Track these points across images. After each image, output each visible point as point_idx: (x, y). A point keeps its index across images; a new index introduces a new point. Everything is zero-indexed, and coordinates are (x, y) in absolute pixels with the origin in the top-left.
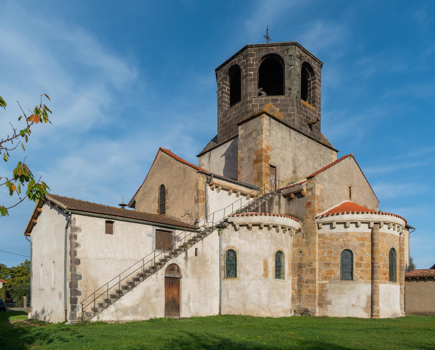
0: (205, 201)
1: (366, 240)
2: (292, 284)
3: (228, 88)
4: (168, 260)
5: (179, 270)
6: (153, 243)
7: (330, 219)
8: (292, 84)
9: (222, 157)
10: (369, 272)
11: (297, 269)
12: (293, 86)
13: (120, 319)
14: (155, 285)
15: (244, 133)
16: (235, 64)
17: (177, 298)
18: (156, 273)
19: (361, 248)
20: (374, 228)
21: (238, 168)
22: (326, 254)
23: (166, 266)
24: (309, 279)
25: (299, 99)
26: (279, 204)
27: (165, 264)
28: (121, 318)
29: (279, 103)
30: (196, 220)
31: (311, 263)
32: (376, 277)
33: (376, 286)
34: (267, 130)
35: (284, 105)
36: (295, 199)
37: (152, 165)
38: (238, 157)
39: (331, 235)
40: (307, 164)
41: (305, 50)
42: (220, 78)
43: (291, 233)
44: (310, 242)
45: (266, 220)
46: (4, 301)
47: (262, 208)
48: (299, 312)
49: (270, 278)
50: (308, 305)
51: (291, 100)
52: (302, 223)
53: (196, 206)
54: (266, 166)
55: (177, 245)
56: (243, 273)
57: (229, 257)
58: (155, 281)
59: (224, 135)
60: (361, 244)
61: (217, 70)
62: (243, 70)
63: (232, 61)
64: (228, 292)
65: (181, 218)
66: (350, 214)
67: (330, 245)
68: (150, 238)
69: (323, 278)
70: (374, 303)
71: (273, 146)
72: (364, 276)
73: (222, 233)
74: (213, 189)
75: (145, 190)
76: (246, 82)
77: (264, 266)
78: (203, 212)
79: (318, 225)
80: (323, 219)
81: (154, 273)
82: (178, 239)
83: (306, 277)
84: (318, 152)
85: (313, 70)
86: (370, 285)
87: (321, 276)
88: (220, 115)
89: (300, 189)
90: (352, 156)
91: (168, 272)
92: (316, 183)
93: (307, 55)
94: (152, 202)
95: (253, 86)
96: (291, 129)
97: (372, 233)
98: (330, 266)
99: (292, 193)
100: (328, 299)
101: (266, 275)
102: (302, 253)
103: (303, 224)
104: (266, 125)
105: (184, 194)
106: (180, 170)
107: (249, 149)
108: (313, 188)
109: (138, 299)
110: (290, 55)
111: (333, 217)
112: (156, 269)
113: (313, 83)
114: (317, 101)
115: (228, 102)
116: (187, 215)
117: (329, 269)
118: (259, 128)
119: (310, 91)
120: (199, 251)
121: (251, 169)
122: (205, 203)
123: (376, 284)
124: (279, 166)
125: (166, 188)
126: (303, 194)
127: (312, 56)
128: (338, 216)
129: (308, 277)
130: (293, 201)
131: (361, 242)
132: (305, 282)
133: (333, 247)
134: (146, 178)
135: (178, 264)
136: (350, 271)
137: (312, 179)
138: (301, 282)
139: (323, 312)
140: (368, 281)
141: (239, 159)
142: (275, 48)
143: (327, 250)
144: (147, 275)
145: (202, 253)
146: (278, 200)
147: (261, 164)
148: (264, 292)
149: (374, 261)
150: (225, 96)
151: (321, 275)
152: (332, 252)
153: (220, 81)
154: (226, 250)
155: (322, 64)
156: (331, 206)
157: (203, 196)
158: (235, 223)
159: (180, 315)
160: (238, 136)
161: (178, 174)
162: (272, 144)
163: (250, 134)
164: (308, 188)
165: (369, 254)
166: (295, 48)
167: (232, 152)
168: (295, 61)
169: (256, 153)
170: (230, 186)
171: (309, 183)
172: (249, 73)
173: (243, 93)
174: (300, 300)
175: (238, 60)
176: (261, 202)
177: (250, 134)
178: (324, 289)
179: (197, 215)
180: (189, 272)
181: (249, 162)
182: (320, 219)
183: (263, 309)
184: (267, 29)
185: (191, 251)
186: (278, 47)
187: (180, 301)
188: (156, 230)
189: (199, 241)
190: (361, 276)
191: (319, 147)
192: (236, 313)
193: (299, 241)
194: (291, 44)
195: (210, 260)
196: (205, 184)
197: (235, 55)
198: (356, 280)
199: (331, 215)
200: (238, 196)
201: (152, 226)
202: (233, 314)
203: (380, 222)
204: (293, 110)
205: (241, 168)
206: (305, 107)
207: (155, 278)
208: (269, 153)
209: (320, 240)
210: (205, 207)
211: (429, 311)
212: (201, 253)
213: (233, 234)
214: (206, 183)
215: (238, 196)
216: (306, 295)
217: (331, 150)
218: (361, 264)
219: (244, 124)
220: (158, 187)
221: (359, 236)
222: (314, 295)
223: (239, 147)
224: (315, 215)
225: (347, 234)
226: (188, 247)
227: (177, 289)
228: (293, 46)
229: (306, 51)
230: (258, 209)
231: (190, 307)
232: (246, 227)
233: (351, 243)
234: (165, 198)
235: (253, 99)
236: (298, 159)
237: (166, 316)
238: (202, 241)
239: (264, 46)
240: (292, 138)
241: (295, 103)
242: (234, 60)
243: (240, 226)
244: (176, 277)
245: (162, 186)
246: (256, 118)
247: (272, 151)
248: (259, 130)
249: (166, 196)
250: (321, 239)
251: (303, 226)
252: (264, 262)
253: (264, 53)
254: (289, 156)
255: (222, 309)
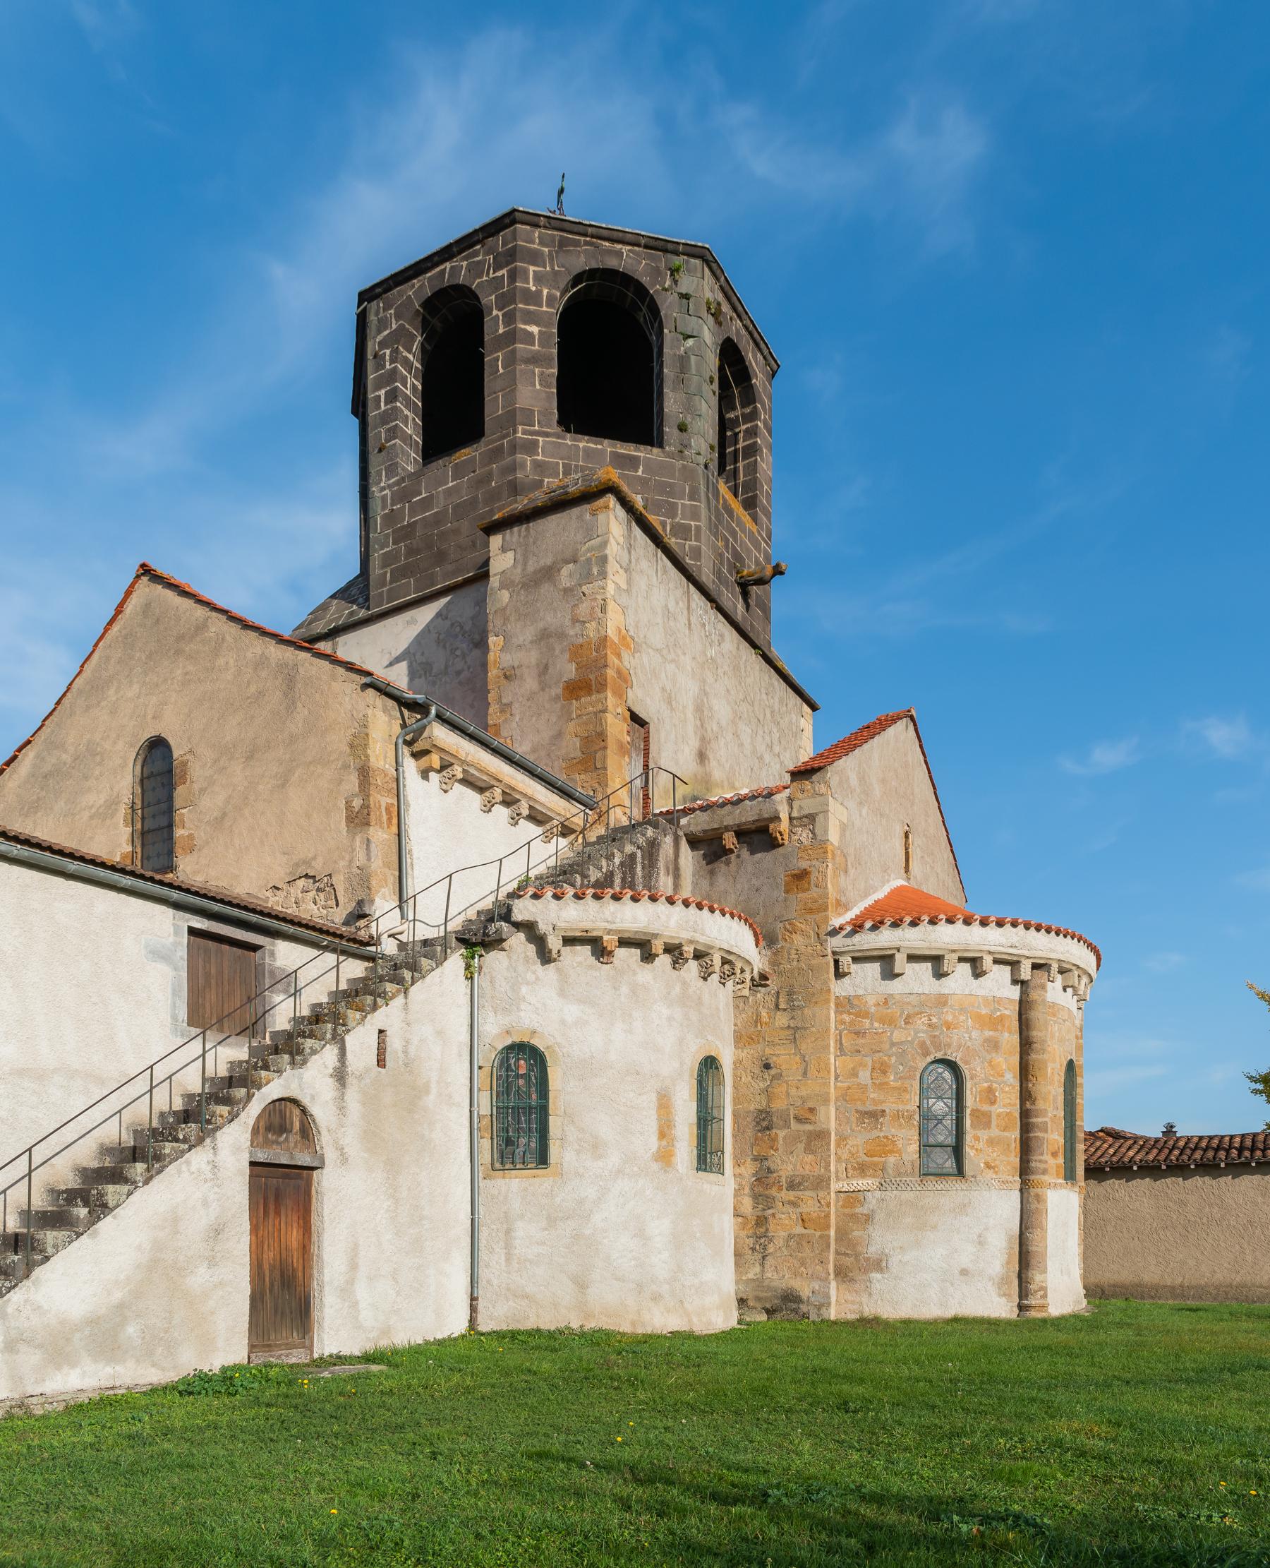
0: (395, 821)
1: (1004, 1026)
2: (738, 1192)
3: (416, 383)
4: (264, 1081)
5: (307, 1132)
6: (175, 993)
7: (886, 938)
8: (689, 408)
9: (391, 664)
10: (1013, 1145)
11: (750, 1132)
12: (693, 419)
13: (30, 1391)
14: (205, 1203)
15: (514, 566)
16: (455, 282)
17: (301, 1261)
18: (208, 1141)
19: (988, 1057)
20: (1032, 985)
21: (491, 710)
22: (865, 1076)
23: (254, 1109)
24: (801, 1172)
25: (713, 476)
26: (676, 873)
27: (249, 1097)
28: (36, 1382)
29: (640, 473)
30: (360, 903)
31: (812, 1110)
32: (1038, 1165)
33: (1038, 1197)
34: (621, 567)
35: (662, 488)
36: (738, 856)
37: (96, 645)
38: (491, 666)
39: (886, 1002)
40: (736, 735)
41: (730, 292)
42: (379, 332)
43: (739, 986)
44: (805, 1029)
45: (672, 923)
46: (833, 1284)
47: (623, 879)
48: (759, 1306)
49: (679, 1167)
50: (796, 1274)
51: (688, 474)
52: (769, 953)
53: (358, 839)
54: (619, 710)
55: (282, 1015)
56: (576, 1146)
57: (508, 1076)
58: (206, 1181)
59: (404, 576)
60: (987, 1040)
61: (366, 296)
62: (495, 312)
63: (442, 267)
64: (508, 1232)
65: (268, 894)
66: (959, 924)
67: (881, 1042)
68: (163, 968)
69: (854, 1169)
70: (1033, 1262)
71: (638, 637)
72: (997, 1162)
73: (480, 968)
74: (425, 774)
75: (54, 761)
76: (511, 361)
77: (659, 1119)
78: (387, 871)
79: (836, 962)
80: (857, 938)
81: (201, 1140)
82: (290, 982)
83: (787, 1164)
84: (764, 696)
85: (751, 380)
86: (1016, 1195)
87: (847, 1161)
88: (383, 489)
89: (766, 816)
90: (912, 718)
91: (261, 1139)
92: (830, 798)
93: (734, 315)
94: (91, 818)
95: (538, 387)
96: (690, 585)
97: (1021, 1001)
98: (882, 1124)
99: (727, 829)
100: (873, 1250)
101: (665, 1157)
102: (773, 1072)
103: (775, 954)
104: (618, 544)
105: (283, 785)
106: (264, 674)
107: (544, 636)
108: (817, 814)
109: (122, 1277)
110: (684, 292)
111: (898, 933)
112: (209, 1122)
113: (746, 431)
114: (761, 501)
115: (416, 442)
116: (301, 882)
117: (876, 1133)
118: (588, 550)
119: (736, 461)
120: (394, 1044)
121: (554, 719)
122: (394, 829)
123: (1039, 1191)
124: (656, 720)
125: (175, 755)
126: (778, 835)
127: (749, 321)
128: (917, 928)
129: (799, 1166)
130: (728, 863)
131: (988, 1033)
132: (785, 1185)
133: (891, 1048)
134: (58, 703)
135: (306, 1101)
136: (951, 1140)
137: (815, 778)
138: (767, 1186)
139: (853, 1303)
140: (1010, 1178)
141: (493, 673)
142: (625, 249)
143: (869, 1060)
144: (167, 1151)
145: (405, 1052)
146: (671, 851)
147: (599, 700)
148: (660, 1229)
149: (1033, 1107)
150: (406, 412)
151: (845, 1156)
152: (889, 1067)
153: (383, 344)
154: (500, 1047)
155: (775, 367)
156: (866, 895)
157: (389, 801)
158: (543, 927)
159: (312, 1345)
160: (482, 575)
161: (253, 689)
162: (637, 626)
163: (548, 574)
164: (795, 814)
165: (1011, 1078)
166: (699, 269)
167: (444, 647)
168: (701, 321)
169: (576, 652)
170: (494, 771)
171: (799, 795)
172: (523, 326)
173: (494, 407)
174: (764, 1258)
175: (469, 269)
176: (622, 852)
177: (548, 574)
178: (857, 1210)
179: (363, 879)
180: (351, 1140)
181: (543, 689)
182: (845, 937)
183: (656, 1298)
184: (561, 191)
185: (360, 1040)
186: (636, 248)
187: (311, 1277)
188: (192, 931)
189: (391, 999)
190: (989, 1159)
191: (766, 678)
192: (548, 1322)
193: (757, 1020)
194: (689, 249)
195: (434, 1090)
196: (396, 745)
197: (458, 242)
198: (973, 1176)
199: (889, 923)
200: (514, 821)
201: (170, 912)
202: (529, 1325)
203: (1048, 962)
204: (695, 515)
205: (502, 711)
206: (730, 512)
207: (206, 1168)
208: (628, 661)
209: (843, 1023)
210: (395, 850)
211: (1112, 1282)
212: (400, 1054)
213: (533, 976)
214: (400, 741)
215: (514, 821)
216: (791, 1237)
217: (799, 700)
218: (988, 1115)
219: (516, 529)
220: (131, 746)
221: (984, 1012)
222: (820, 1237)
223: (494, 623)
224: (826, 919)
225: (942, 1001)
226: (351, 1024)
227: (301, 1222)
228: (693, 260)
229: (734, 299)
230: (612, 882)
231: (357, 1303)
232: (587, 950)
233: (956, 1037)
234: (170, 799)
235: (541, 439)
236: (711, 709)
237: (253, 1356)
238: (406, 998)
239: (581, 229)
240: (693, 619)
241: (703, 488)
242: (448, 265)
243: (569, 941)
244: (299, 1163)
245: (157, 747)
246: (575, 511)
247: (636, 655)
248: (589, 560)
249: (180, 793)
250: (846, 1018)
251: (773, 963)
252: (658, 1100)
253: (581, 260)
254: (688, 690)
255: (481, 1305)
